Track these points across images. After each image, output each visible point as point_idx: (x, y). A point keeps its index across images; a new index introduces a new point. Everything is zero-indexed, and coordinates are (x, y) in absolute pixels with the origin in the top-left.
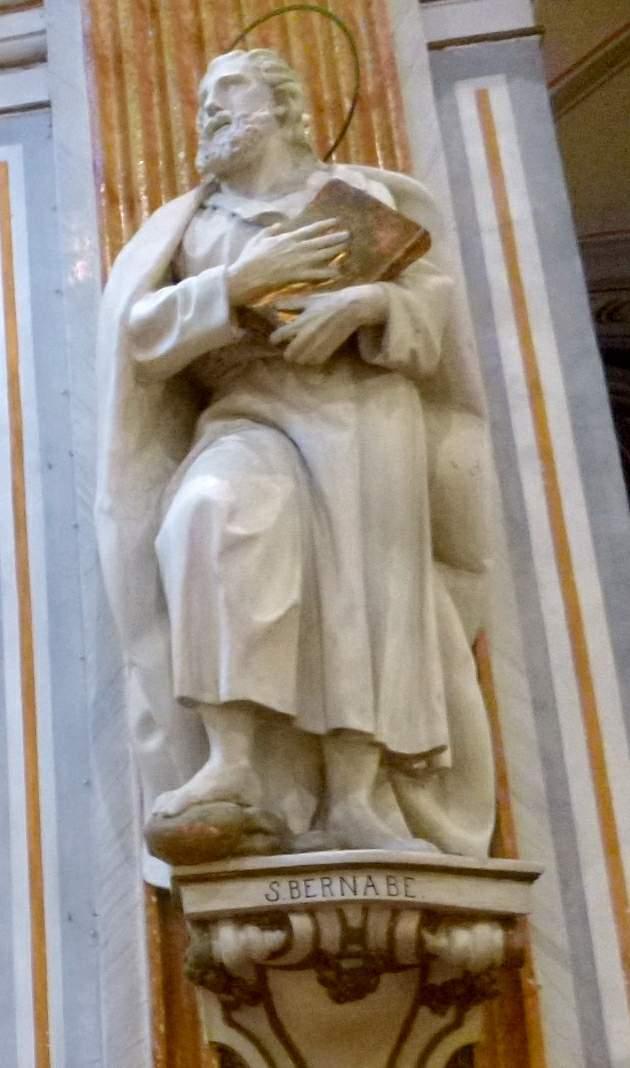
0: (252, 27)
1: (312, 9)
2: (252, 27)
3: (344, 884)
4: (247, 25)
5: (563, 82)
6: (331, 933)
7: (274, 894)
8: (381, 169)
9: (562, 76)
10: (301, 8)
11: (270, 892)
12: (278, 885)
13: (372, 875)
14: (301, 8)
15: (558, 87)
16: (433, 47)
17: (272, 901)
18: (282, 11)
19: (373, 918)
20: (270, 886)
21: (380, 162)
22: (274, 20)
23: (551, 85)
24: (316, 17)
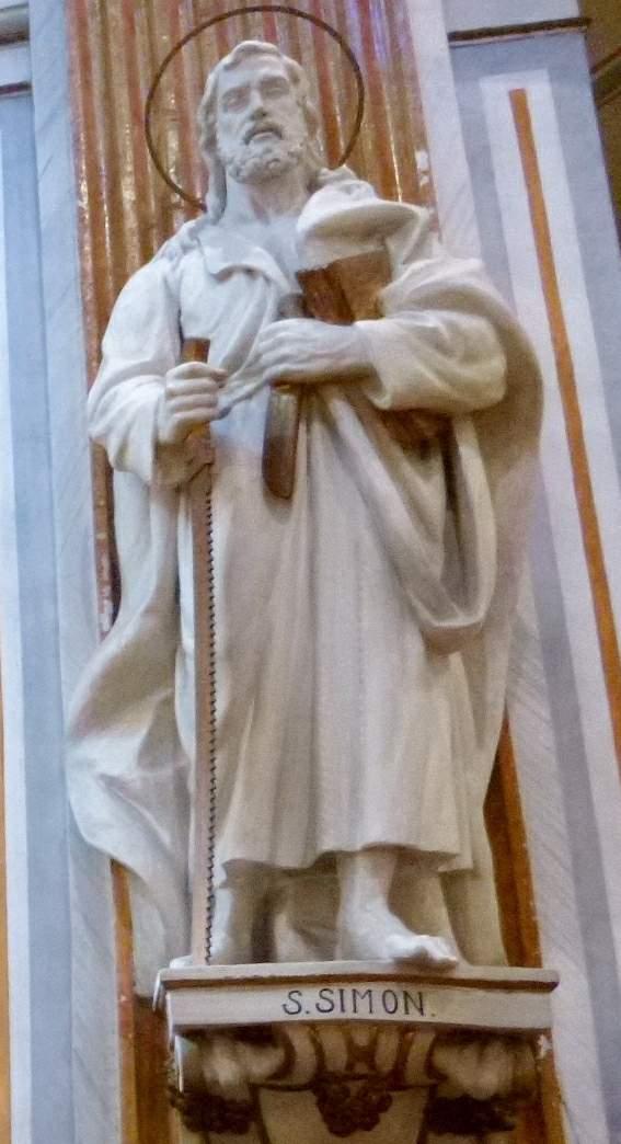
0: (188, 38)
1: (300, 14)
2: (188, 38)
3: (408, 1000)
4: (182, 36)
5: (608, 68)
6: (338, 1058)
7: (327, 1003)
8: (400, 203)
9: (605, 62)
10: (265, 9)
11: (289, 1002)
12: (300, 994)
13: (423, 990)
14: (244, 11)
15: (600, 73)
16: (454, 37)
17: (325, 1011)
18: (219, 19)
19: (383, 1039)
20: (321, 996)
21: (400, 197)
22: (211, 30)
23: (594, 70)
24: (305, 26)
